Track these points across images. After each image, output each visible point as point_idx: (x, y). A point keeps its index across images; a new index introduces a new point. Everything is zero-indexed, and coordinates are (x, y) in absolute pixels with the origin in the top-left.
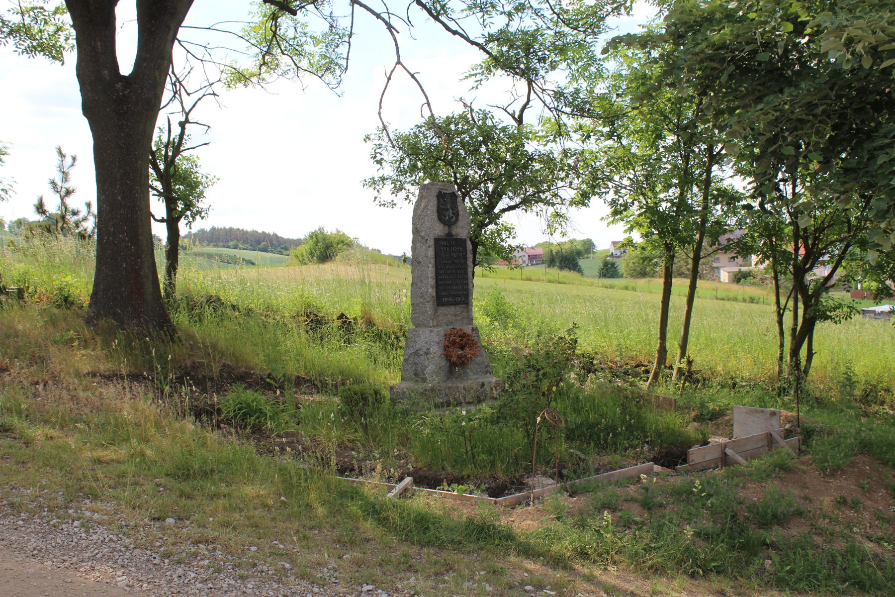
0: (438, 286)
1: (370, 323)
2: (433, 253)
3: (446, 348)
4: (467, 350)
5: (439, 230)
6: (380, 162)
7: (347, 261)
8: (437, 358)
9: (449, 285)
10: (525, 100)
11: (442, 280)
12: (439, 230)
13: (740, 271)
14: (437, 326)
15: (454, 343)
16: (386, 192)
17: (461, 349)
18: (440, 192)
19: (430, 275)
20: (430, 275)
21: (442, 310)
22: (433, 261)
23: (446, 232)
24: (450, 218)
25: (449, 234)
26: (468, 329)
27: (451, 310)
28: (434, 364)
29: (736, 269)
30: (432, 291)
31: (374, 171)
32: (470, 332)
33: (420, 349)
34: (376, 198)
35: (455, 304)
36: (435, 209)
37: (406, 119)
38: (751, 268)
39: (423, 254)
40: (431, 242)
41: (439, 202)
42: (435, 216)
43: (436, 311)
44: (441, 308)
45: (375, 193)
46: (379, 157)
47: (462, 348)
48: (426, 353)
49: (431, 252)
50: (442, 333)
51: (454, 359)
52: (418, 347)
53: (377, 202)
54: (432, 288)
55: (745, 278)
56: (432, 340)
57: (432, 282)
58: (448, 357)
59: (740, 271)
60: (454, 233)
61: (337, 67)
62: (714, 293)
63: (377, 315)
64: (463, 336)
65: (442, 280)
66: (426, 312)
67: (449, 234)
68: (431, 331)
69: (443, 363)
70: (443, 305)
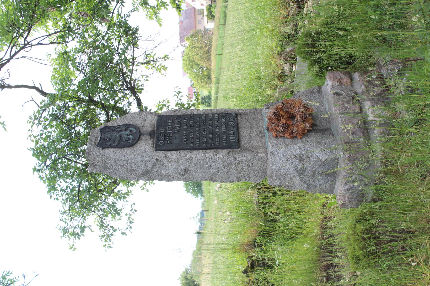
0: (214, 148)
1: (253, 245)
2: (174, 152)
3: (293, 136)
4: (295, 111)
5: (145, 146)
6: (83, 229)
7: (199, 274)
8: (307, 147)
9: (214, 134)
10: (34, 91)
11: (207, 142)
12: (145, 146)
13: (207, 16)
14: (265, 147)
15: (287, 127)
16: (119, 223)
17: (293, 120)
18: (99, 145)
19: (202, 156)
20: (202, 156)
21: (244, 142)
22: (183, 153)
23: (148, 137)
24: (131, 133)
25: (152, 134)
26: (268, 113)
27: (244, 132)
28: (315, 151)
29: (206, 18)
30: (222, 154)
31: (93, 234)
32: (272, 111)
33: (296, 167)
34: (123, 233)
35: (237, 127)
36: (118, 151)
37: (49, 207)
38: (205, 9)
39: (175, 165)
40: (160, 155)
41: (111, 146)
42: (128, 151)
43: (247, 149)
44: (242, 143)
45: (118, 233)
46: (78, 231)
47: (293, 117)
48: (301, 159)
49: (173, 155)
50: (274, 141)
51: (307, 125)
52: (292, 171)
53: (127, 232)
54: (217, 153)
55: (211, 12)
56: (282, 157)
57: (210, 154)
58: (305, 133)
59: (207, 16)
60: (149, 130)
61: (8, 278)
62: (221, 26)
63: (244, 238)
64: (277, 115)
65: (207, 142)
66: (247, 161)
67: (152, 134)
68: (272, 154)
69: (312, 138)
70: (239, 141)
